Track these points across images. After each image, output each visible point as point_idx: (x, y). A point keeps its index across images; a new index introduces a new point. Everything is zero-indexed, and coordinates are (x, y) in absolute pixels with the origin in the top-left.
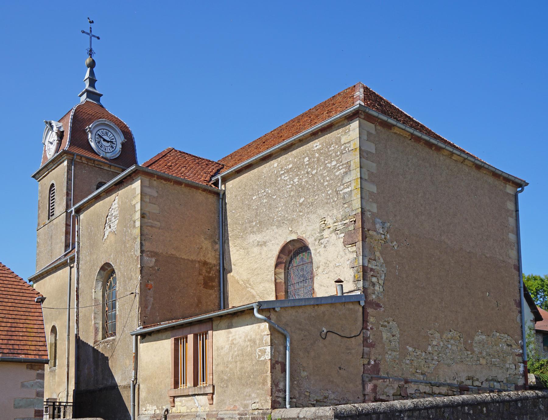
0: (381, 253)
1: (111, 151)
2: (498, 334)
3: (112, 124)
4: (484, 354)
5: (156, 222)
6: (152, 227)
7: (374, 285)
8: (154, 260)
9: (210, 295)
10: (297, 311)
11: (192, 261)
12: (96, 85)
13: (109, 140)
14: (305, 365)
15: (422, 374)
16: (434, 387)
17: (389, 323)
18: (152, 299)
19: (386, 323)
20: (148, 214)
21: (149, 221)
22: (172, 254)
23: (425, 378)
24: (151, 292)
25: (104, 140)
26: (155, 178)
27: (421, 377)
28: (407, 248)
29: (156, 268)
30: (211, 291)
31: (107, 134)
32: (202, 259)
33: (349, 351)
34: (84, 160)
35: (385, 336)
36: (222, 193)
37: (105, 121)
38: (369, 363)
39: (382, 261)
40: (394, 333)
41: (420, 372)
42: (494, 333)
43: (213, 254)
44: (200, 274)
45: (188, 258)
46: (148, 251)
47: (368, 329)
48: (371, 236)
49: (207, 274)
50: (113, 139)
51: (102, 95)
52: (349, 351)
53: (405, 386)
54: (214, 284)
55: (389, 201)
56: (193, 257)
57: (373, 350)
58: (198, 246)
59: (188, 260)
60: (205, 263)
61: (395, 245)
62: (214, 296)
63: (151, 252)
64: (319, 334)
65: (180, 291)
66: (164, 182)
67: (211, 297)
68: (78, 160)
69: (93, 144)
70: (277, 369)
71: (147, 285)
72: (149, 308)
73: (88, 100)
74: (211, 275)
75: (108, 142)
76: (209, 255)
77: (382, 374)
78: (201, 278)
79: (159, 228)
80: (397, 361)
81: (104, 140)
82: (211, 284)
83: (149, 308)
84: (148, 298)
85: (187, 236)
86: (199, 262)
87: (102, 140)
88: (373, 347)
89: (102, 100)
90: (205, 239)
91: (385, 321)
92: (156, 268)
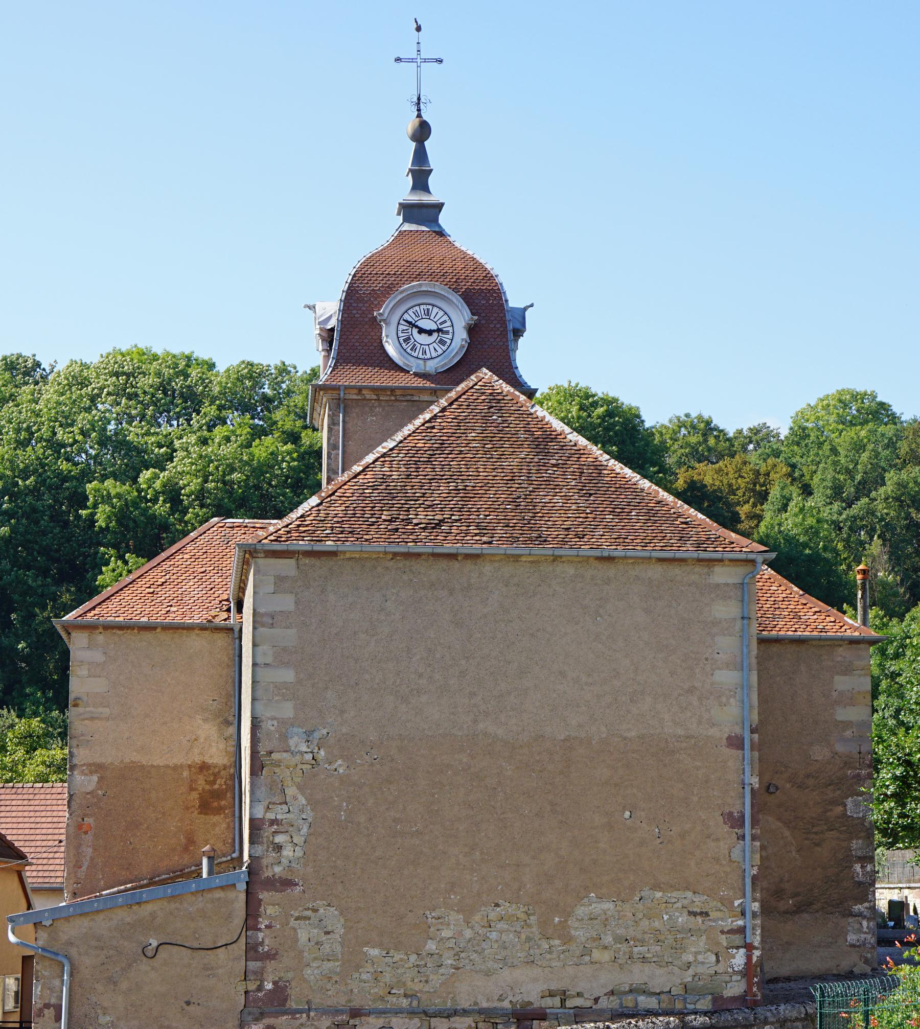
0: (300, 788)
1: (440, 352)
2: (659, 894)
3: (438, 288)
4: (608, 939)
5: (100, 710)
6: (92, 719)
7: (279, 848)
8: (95, 778)
9: (214, 825)
10: (93, 920)
11: (175, 768)
12: (432, 181)
13: (434, 327)
14: (106, 1004)
15: (406, 996)
16: (433, 1020)
17: (315, 911)
18: (90, 850)
19: (309, 913)
20: (85, 698)
21: (87, 709)
22: (132, 762)
23: (415, 1003)
24: (89, 838)
25: (421, 331)
26: (101, 630)
27: (405, 1003)
28: (372, 765)
29: (100, 792)
30: (215, 819)
31: (428, 313)
32: (198, 759)
33: (209, 972)
34: (368, 395)
35: (303, 936)
36: (237, 630)
37: (420, 285)
38: (260, 988)
39: (304, 802)
40: (330, 929)
41: (402, 991)
42: (646, 893)
43: (222, 746)
44: (192, 789)
45: (166, 763)
46: (84, 765)
47: (260, 930)
48: (277, 764)
49: (207, 787)
50: (445, 322)
51: (443, 204)
52: (209, 972)
53: (352, 1022)
54: (223, 803)
55: (326, 688)
56: (179, 759)
57: (270, 965)
58: (188, 738)
59: (167, 766)
60: (204, 767)
61: (340, 766)
62: (224, 825)
63: (90, 765)
64: (140, 951)
65: (148, 828)
66: (118, 632)
67: (217, 829)
68: (355, 397)
69: (391, 349)
70: (47, 1015)
71: (80, 827)
72: (84, 868)
73: (407, 227)
74: (216, 787)
75: (430, 333)
76: (214, 750)
77: (292, 1004)
78: (195, 795)
79: (108, 719)
80: (336, 978)
81: (421, 331)
82: (216, 804)
83: (84, 868)
84: (84, 848)
85: (165, 723)
86: (190, 766)
87: (415, 331)
88: (274, 959)
89: (444, 220)
90: (205, 720)
91: (308, 909)
92: (100, 792)
